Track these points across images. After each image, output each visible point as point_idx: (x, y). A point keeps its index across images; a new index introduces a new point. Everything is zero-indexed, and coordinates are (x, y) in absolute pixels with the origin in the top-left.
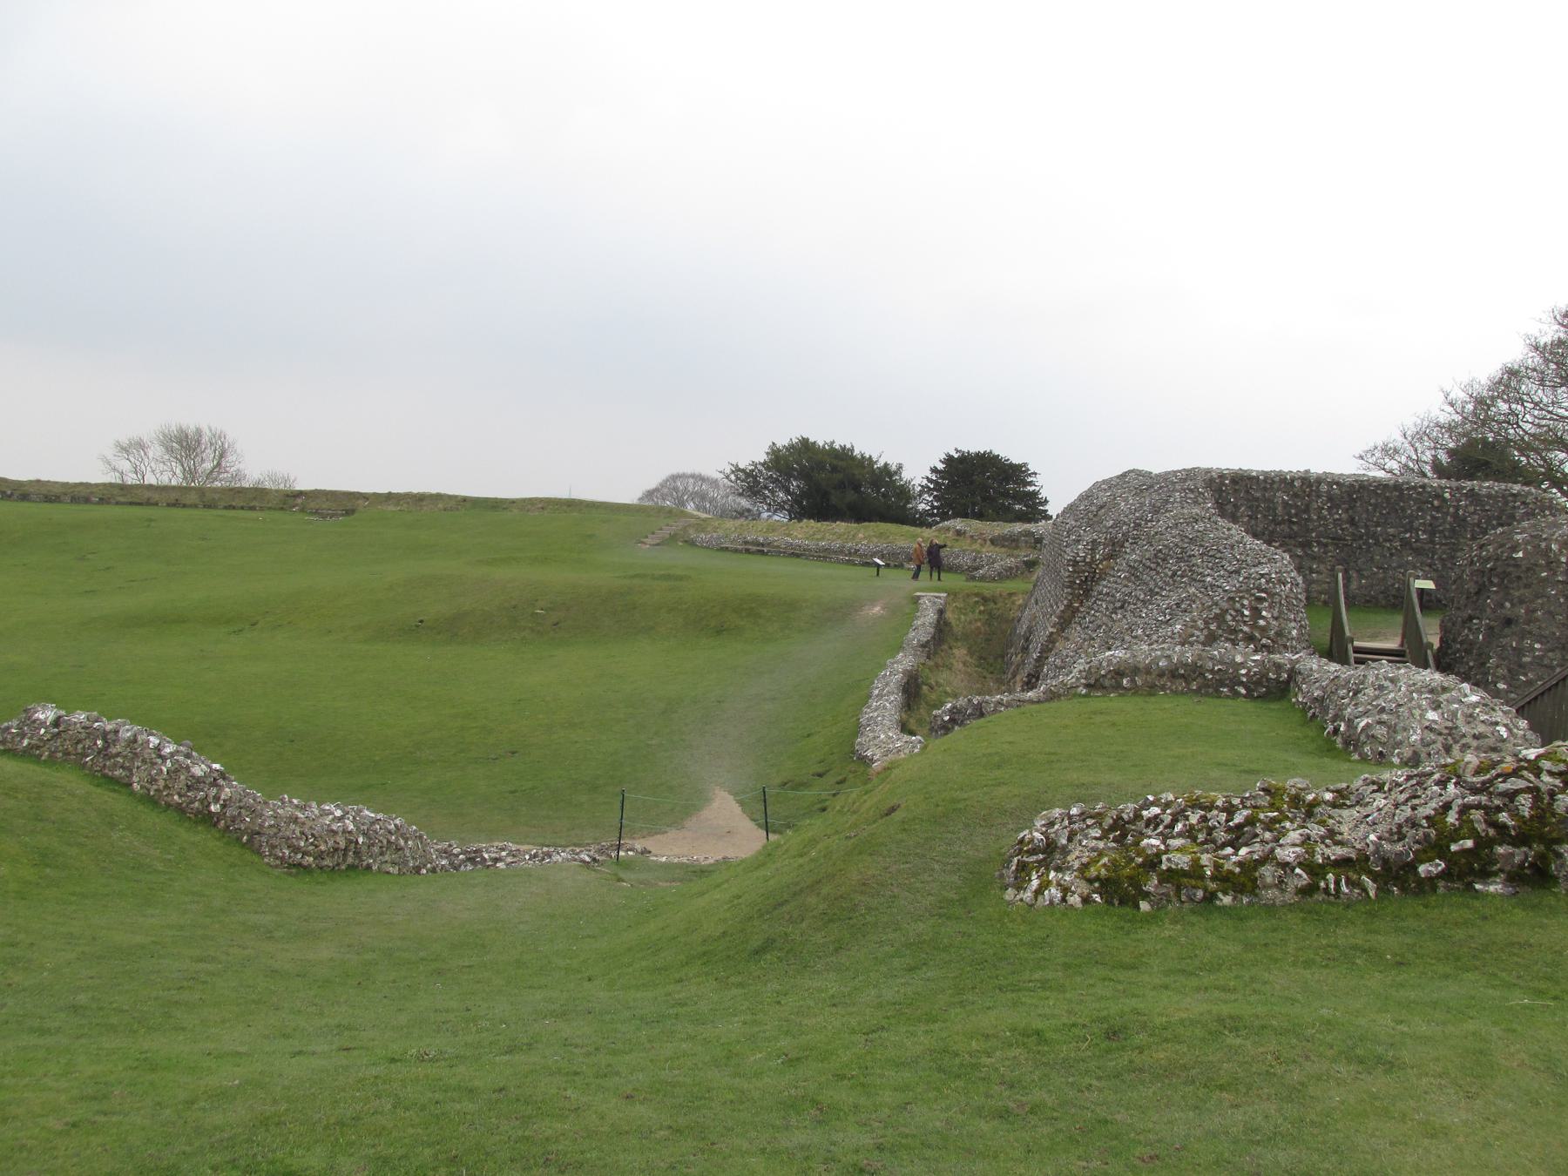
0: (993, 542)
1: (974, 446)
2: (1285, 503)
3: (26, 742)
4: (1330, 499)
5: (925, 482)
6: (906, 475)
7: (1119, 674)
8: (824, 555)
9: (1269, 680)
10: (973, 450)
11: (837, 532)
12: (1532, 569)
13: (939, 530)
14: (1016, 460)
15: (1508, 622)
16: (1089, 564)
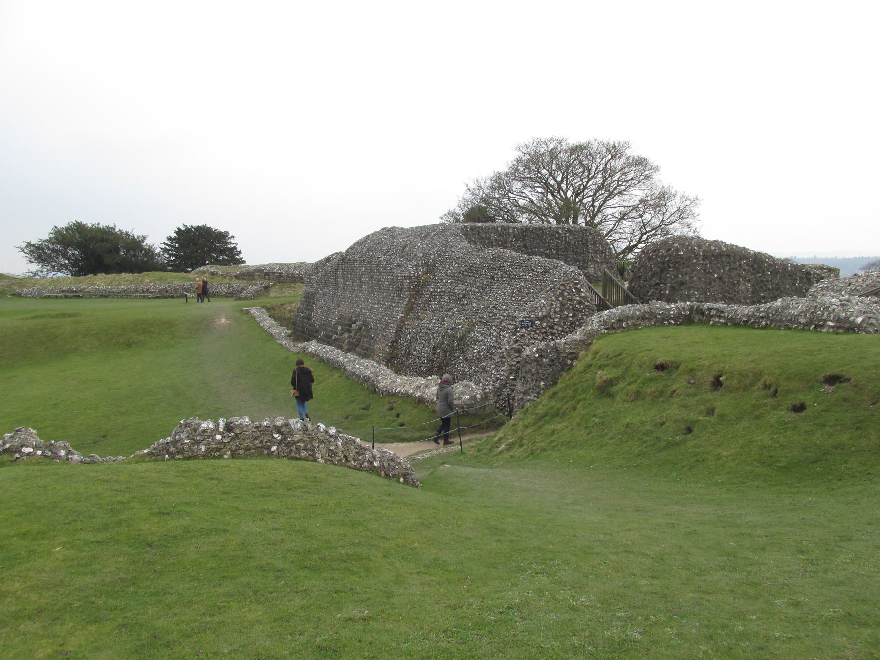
0: (237, 277)
1: (195, 221)
2: (496, 239)
3: (203, 448)
4: (514, 236)
5: (163, 246)
6: (148, 242)
7: (620, 321)
8: (125, 294)
9: (682, 315)
10: (195, 225)
11: (101, 281)
12: (689, 259)
13: (198, 273)
14: (222, 230)
15: (682, 283)
16: (417, 278)
